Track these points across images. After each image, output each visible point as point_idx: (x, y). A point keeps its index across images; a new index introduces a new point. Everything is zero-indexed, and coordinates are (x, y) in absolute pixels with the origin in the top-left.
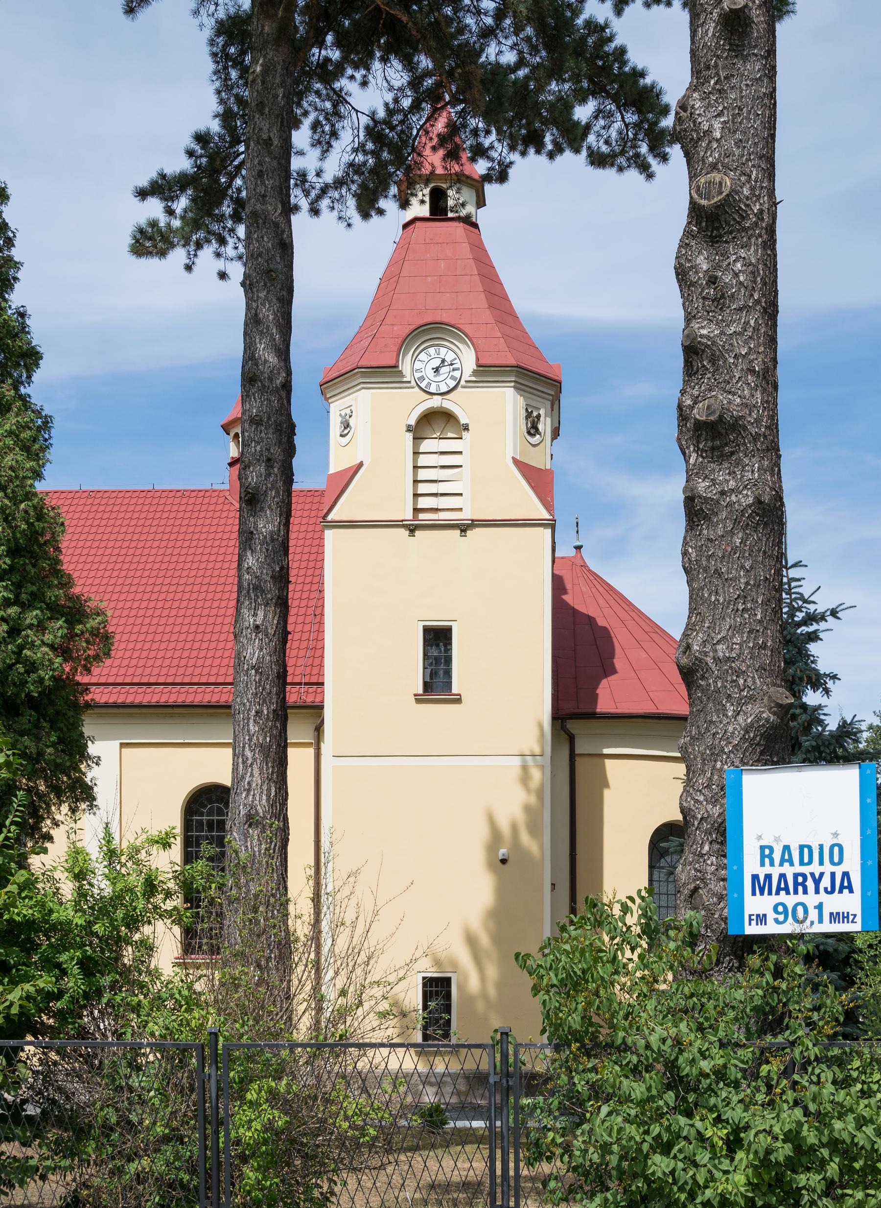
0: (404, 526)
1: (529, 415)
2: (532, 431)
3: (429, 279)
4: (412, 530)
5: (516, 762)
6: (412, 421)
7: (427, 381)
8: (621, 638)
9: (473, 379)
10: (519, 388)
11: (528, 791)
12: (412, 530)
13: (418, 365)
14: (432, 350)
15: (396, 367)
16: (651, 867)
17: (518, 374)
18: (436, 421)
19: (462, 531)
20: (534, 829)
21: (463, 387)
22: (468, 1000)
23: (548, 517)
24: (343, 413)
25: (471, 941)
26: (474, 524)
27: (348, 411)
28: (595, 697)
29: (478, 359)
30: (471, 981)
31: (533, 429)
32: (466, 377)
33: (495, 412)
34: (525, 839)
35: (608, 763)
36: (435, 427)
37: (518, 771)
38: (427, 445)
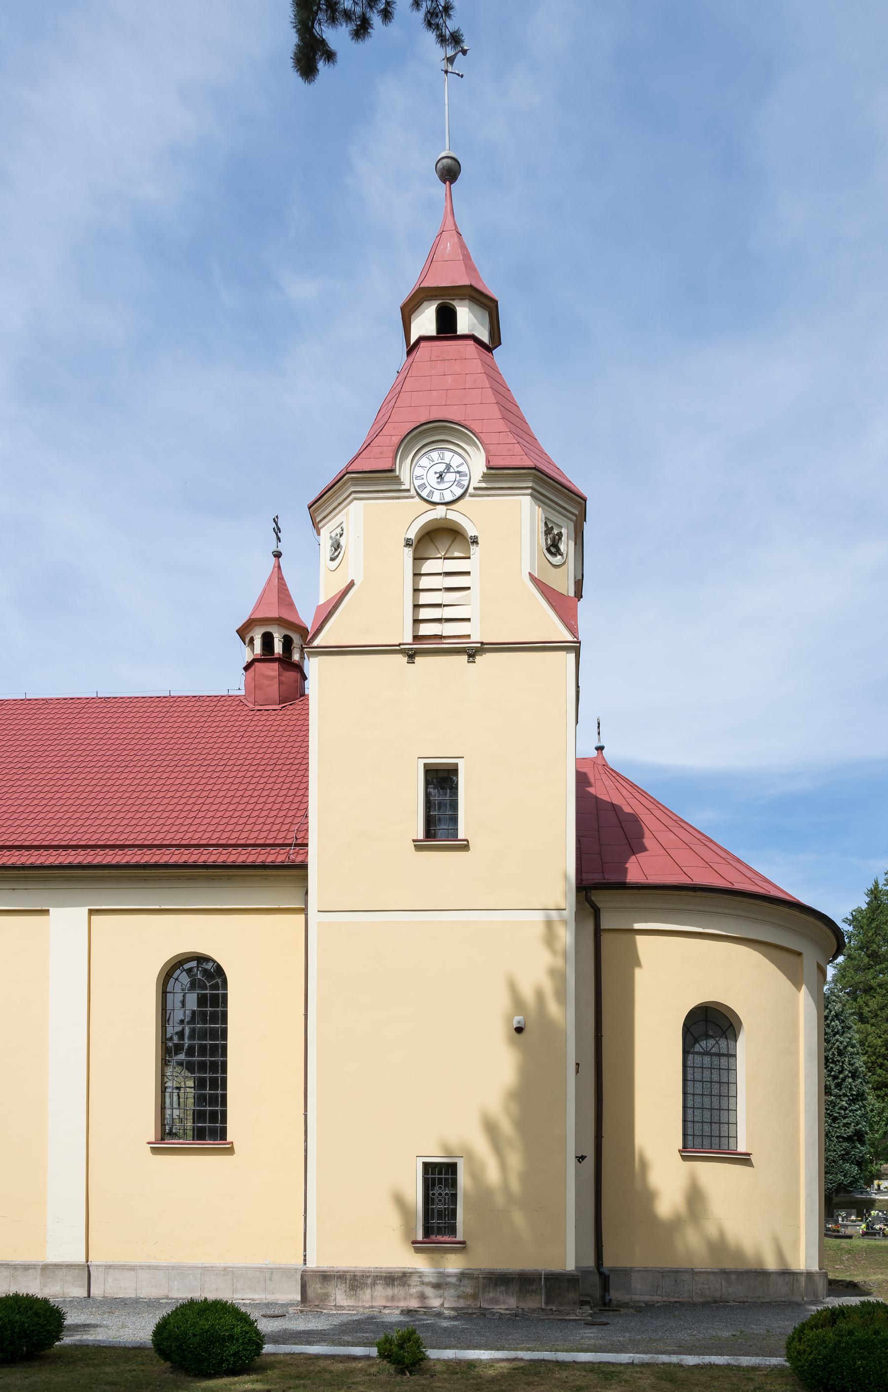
0: (402, 652)
1: (548, 531)
2: (553, 550)
3: (434, 393)
4: (411, 655)
5: (539, 916)
6: (412, 534)
7: (428, 489)
8: (646, 819)
9: (483, 485)
10: (538, 497)
11: (554, 952)
12: (411, 655)
13: (418, 471)
14: (435, 455)
15: (392, 471)
16: (686, 1052)
17: (536, 479)
18: (439, 537)
19: (470, 656)
20: (560, 995)
21: (472, 496)
22: (484, 1193)
23: (571, 638)
24: (333, 535)
25: (491, 1129)
26: (483, 648)
27: (339, 531)
28: (625, 870)
29: (488, 461)
30: (487, 1170)
31: (553, 548)
32: (475, 483)
33: (510, 524)
34: (553, 1008)
35: (639, 939)
36: (439, 547)
37: (540, 929)
38: (428, 566)
